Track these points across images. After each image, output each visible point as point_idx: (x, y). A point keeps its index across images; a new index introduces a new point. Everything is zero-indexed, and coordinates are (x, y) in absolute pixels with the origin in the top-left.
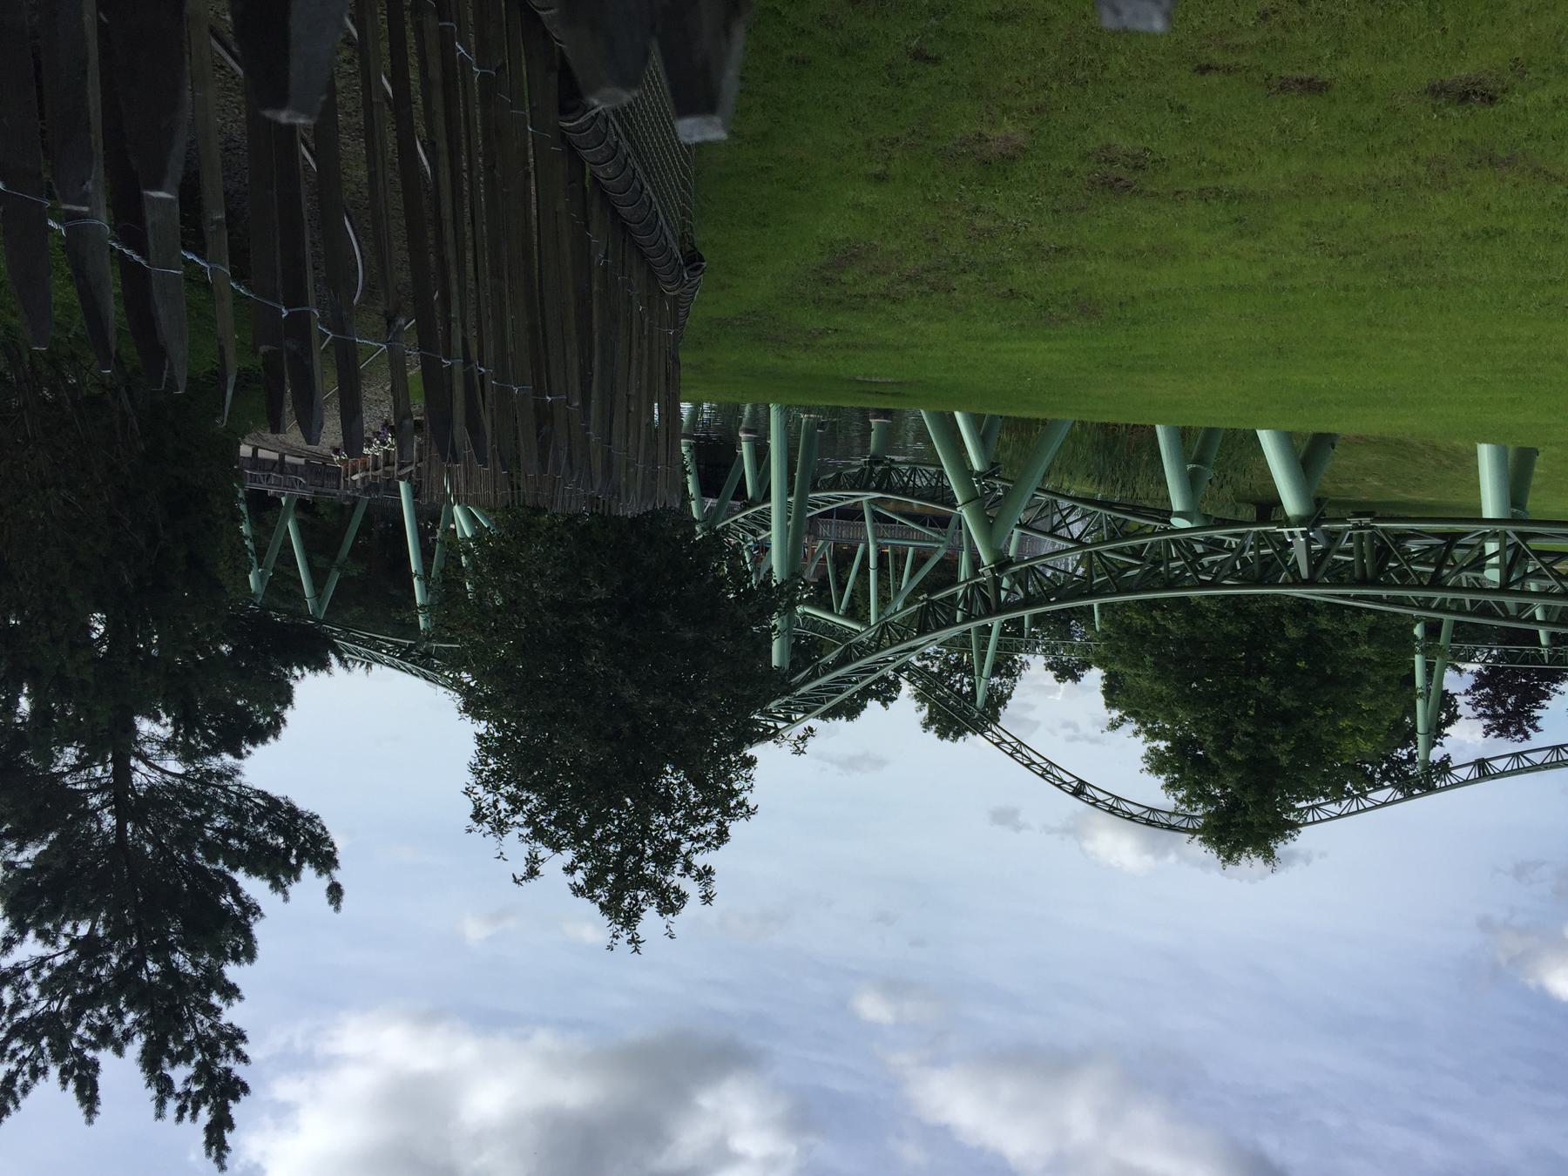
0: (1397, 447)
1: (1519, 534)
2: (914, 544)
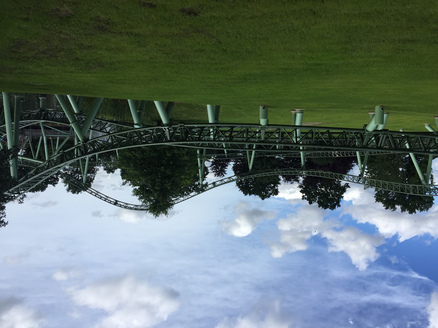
0: (190, 106)
1: (217, 127)
2: (59, 136)
